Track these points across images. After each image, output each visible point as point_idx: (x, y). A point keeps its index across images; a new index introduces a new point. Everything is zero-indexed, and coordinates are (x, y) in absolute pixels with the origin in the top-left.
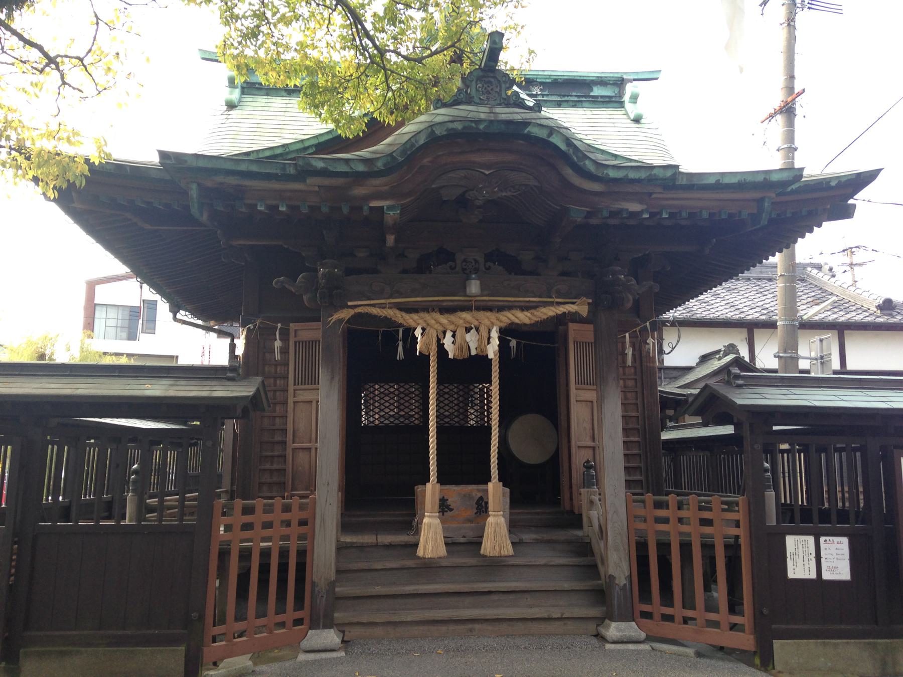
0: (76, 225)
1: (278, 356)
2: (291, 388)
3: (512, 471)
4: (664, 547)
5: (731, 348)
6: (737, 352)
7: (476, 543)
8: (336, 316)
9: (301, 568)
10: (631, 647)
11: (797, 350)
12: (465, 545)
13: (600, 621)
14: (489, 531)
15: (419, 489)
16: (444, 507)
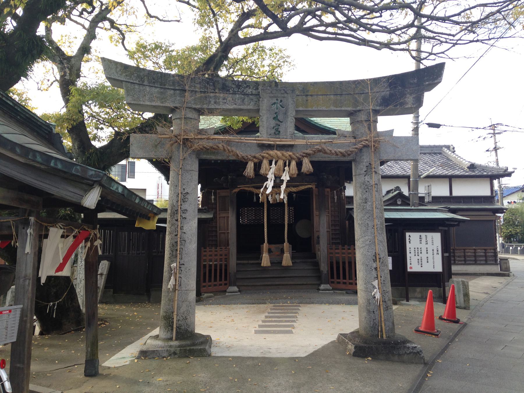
0: (59, 89)
1: (213, 201)
2: (218, 212)
3: (294, 240)
4: (338, 263)
5: (398, 188)
6: (400, 190)
7: (281, 263)
8: (234, 191)
9: (226, 270)
10: (327, 291)
11: (418, 190)
12: (276, 263)
13: (319, 285)
14: (284, 258)
15: (262, 246)
16: (270, 251)
